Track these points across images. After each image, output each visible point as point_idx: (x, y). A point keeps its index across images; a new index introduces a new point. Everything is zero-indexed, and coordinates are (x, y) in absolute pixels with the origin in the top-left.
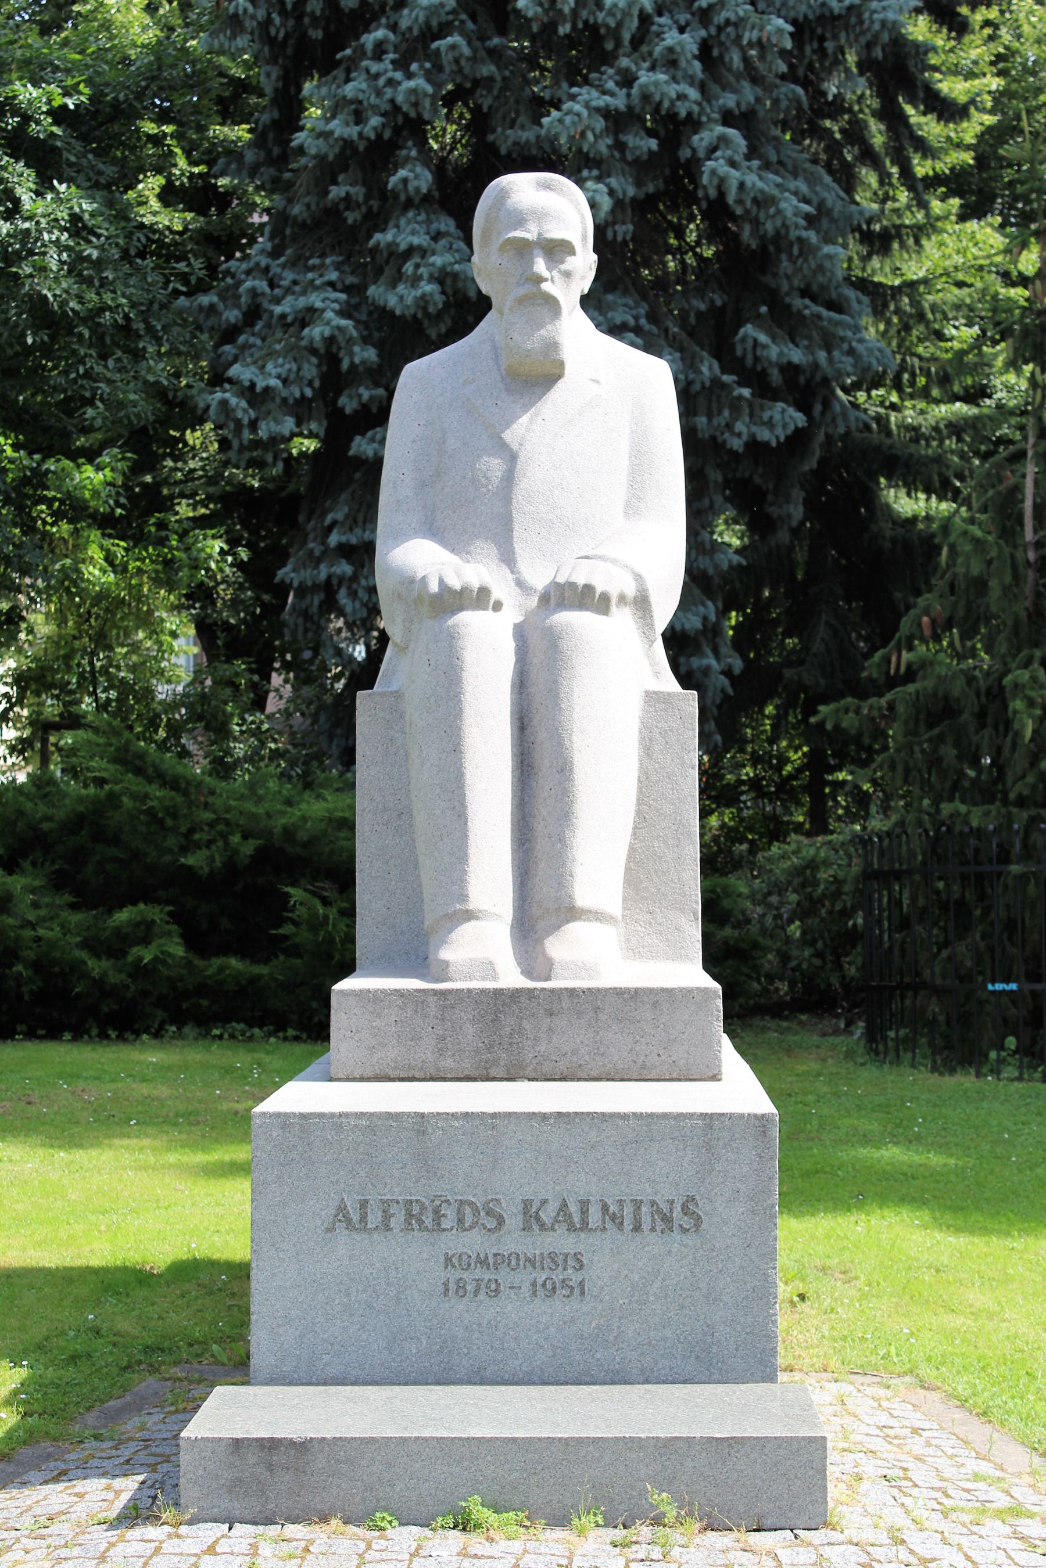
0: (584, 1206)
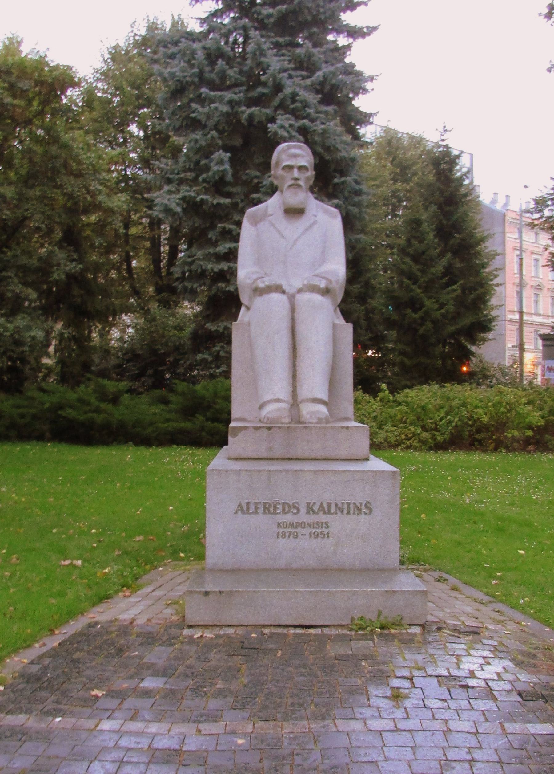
0: (329, 505)
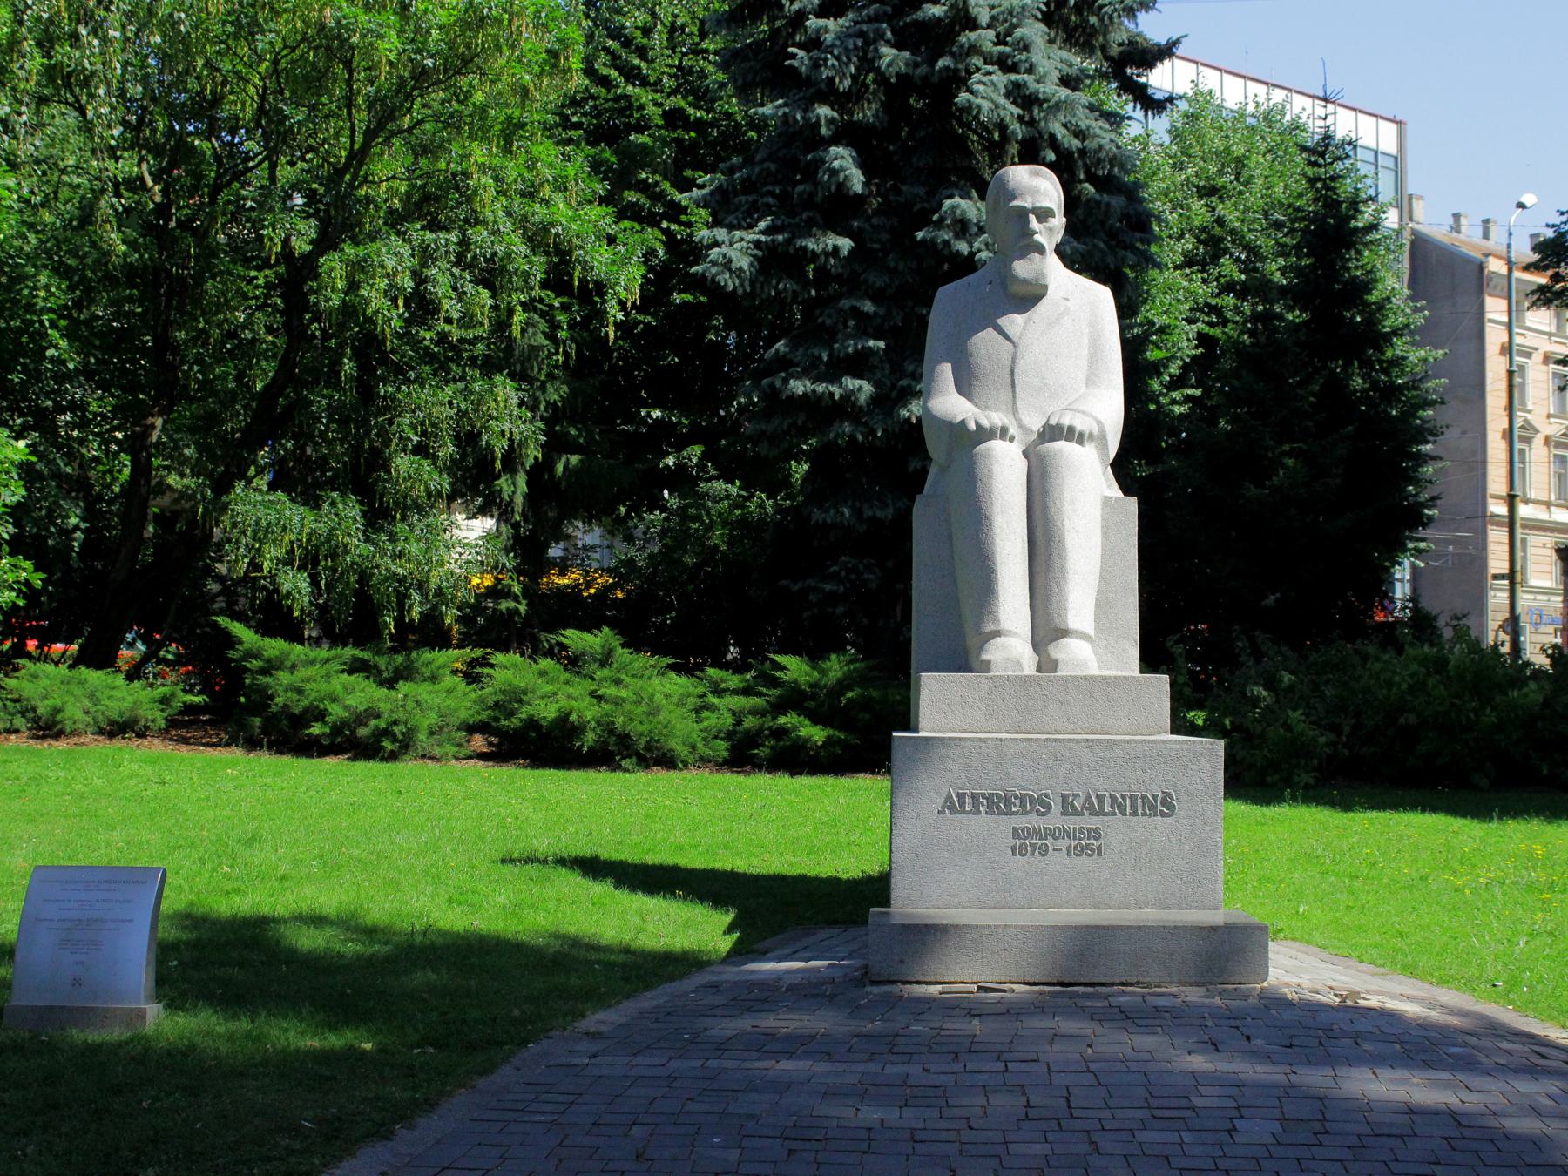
0: (1100, 798)
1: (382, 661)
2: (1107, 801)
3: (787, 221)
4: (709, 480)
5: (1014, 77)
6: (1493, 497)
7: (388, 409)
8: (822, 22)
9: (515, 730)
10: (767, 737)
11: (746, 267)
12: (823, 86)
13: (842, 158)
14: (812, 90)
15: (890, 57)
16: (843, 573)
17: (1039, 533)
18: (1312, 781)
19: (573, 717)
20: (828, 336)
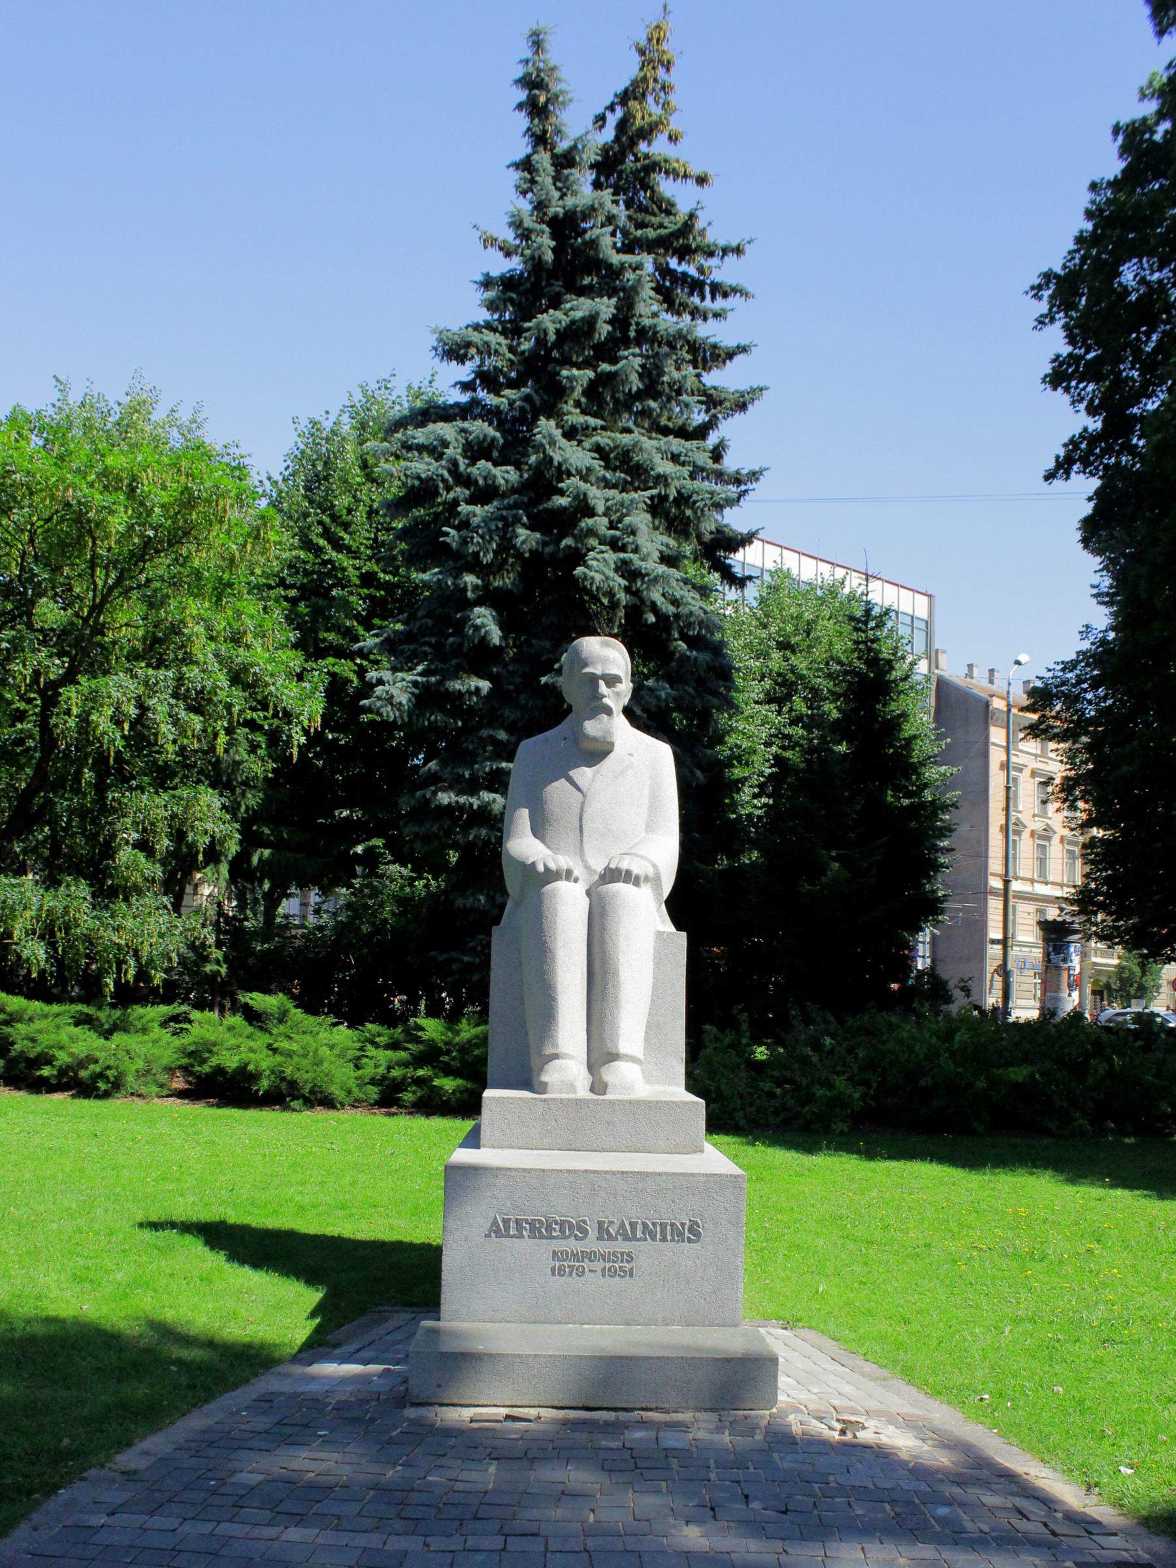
0: (633, 1225)
1: (102, 1015)
2: (639, 1228)
3: (441, 666)
4: (388, 863)
5: (622, 555)
6: (992, 874)
7: (115, 811)
8: (471, 508)
9: (207, 1074)
10: (410, 1084)
11: (404, 702)
12: (469, 558)
13: (484, 618)
14: (462, 562)
15: (526, 537)
16: (479, 948)
17: (597, 965)
18: (846, 1129)
19: (251, 1067)
20: (470, 758)
